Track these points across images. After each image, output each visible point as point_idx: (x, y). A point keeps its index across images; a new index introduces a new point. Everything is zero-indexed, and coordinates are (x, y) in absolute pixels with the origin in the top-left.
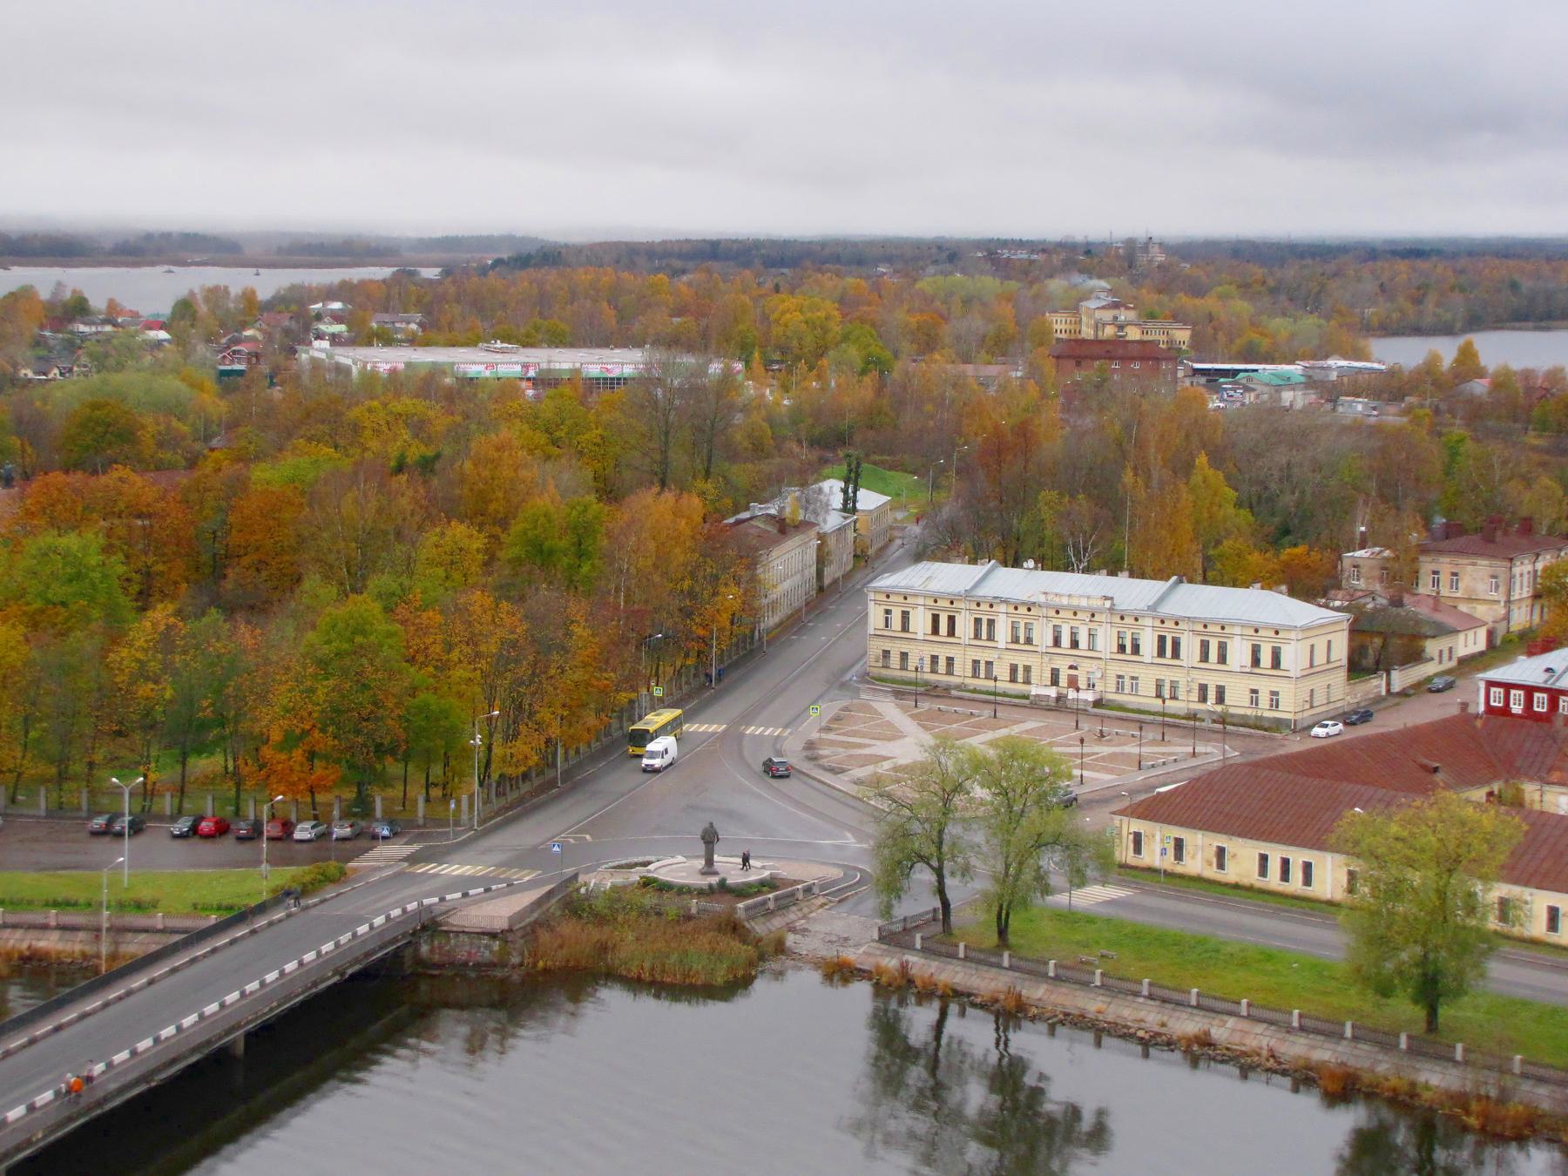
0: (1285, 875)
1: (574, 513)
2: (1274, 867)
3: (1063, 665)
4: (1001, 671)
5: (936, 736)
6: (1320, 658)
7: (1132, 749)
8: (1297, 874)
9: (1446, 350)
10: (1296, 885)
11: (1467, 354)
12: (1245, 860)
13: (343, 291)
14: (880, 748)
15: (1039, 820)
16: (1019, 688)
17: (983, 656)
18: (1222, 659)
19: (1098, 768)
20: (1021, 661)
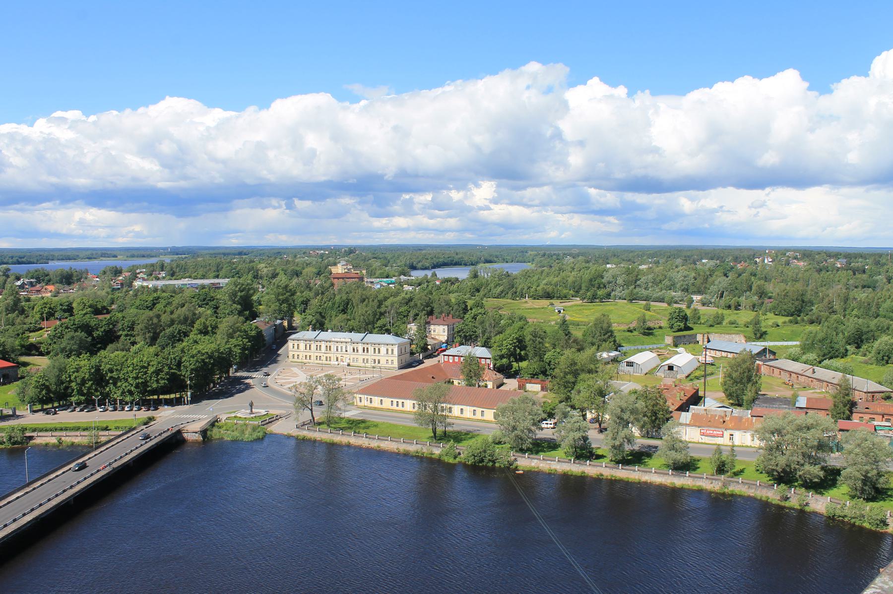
0: (397, 405)
1: (56, 404)
2: (400, 404)
3: (339, 356)
4: (324, 358)
5: (762, 433)
6: (403, 351)
7: (358, 376)
8: (395, 403)
9: (429, 273)
10: (400, 408)
11: (434, 275)
12: (387, 402)
13: (146, 266)
14: (293, 379)
15: (335, 394)
16: (328, 362)
17: (319, 355)
18: (379, 352)
19: (347, 381)
20: (328, 355)
